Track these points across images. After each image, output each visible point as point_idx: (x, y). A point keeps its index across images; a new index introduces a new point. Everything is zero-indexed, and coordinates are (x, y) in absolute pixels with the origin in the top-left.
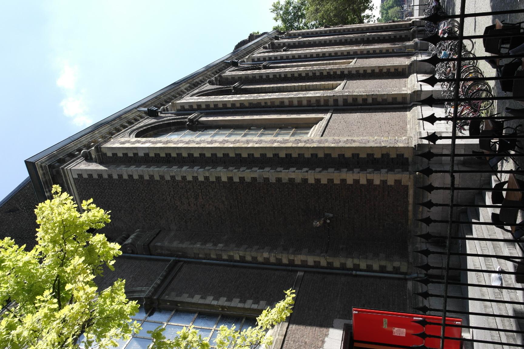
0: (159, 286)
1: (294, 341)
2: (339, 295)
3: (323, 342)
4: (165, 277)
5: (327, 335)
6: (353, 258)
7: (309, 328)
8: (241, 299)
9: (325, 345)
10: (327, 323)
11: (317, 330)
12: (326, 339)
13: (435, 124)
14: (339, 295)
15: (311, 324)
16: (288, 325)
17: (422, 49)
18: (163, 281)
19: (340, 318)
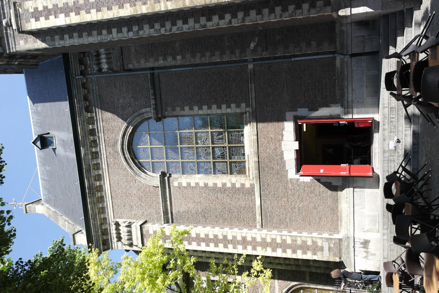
0: (156, 104)
1: (264, 138)
2: (285, 86)
3: (283, 135)
4: (155, 94)
5: (283, 129)
6: (350, 163)
7: (270, 124)
8: (217, 104)
9: (284, 138)
10: (282, 119)
11: (276, 124)
12: (284, 132)
13: (35, 104)
14: (285, 86)
15: (271, 121)
16: (257, 125)
17: (166, 135)
18: (155, 99)
19: (289, 111)
